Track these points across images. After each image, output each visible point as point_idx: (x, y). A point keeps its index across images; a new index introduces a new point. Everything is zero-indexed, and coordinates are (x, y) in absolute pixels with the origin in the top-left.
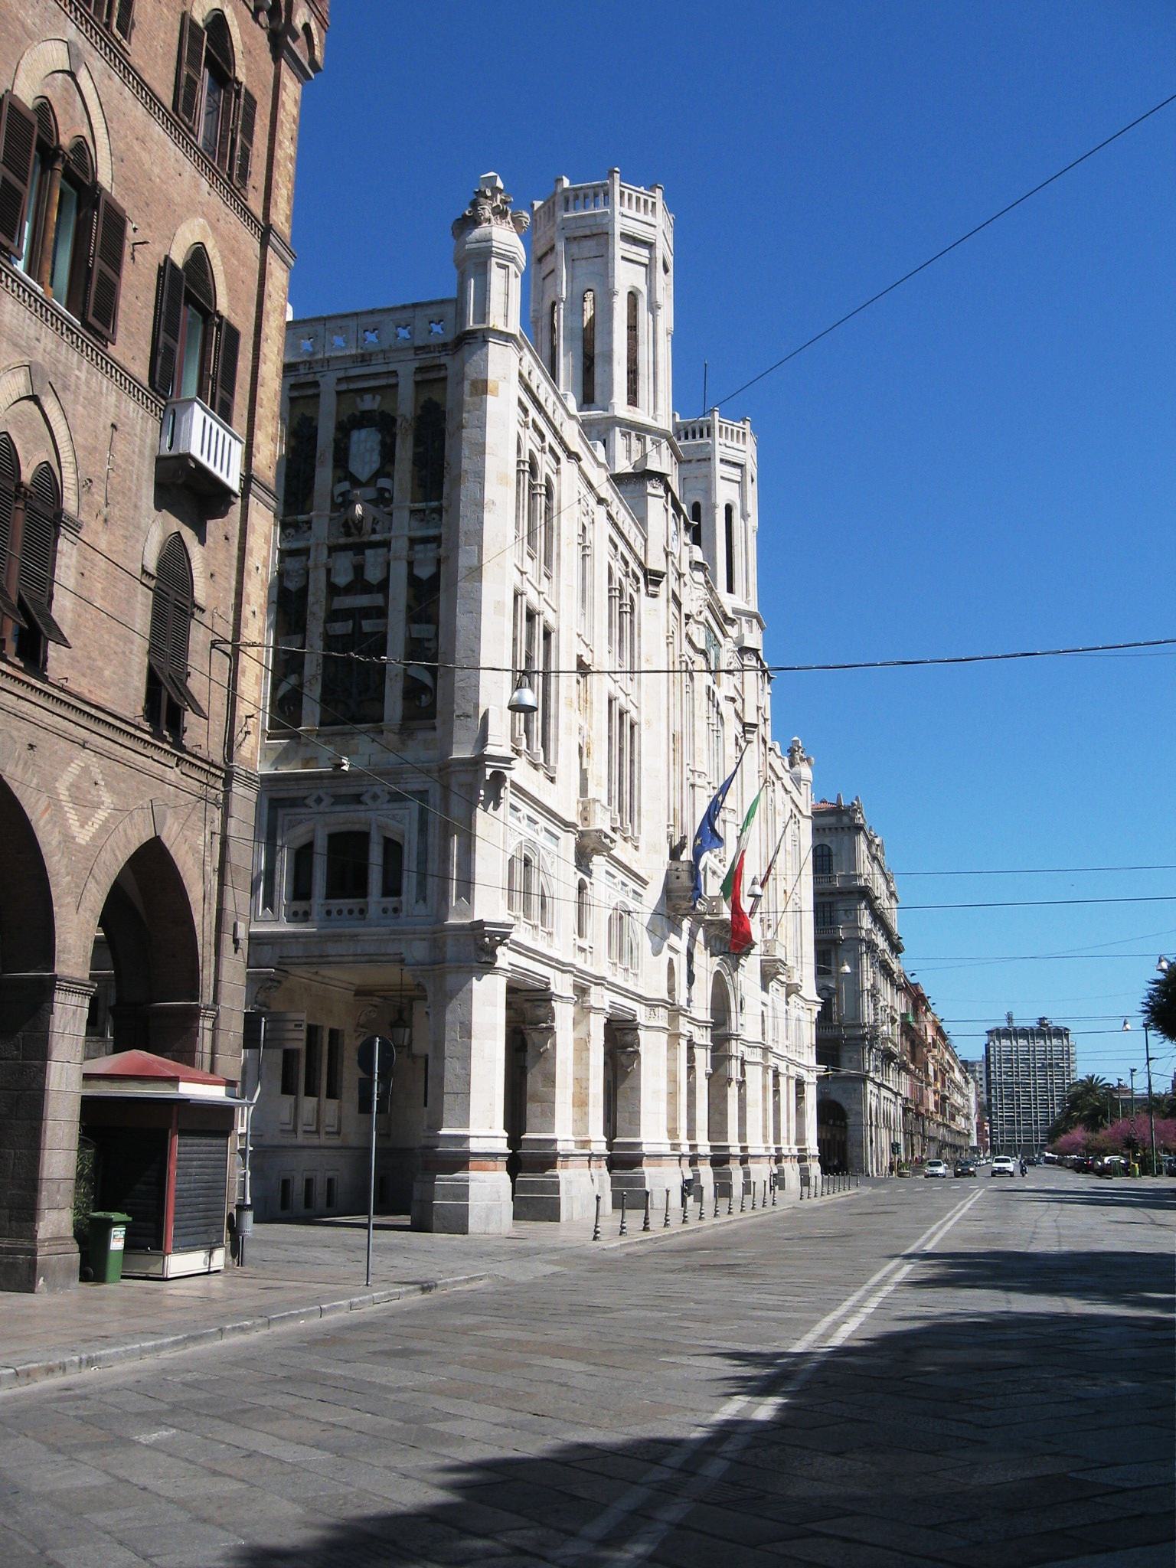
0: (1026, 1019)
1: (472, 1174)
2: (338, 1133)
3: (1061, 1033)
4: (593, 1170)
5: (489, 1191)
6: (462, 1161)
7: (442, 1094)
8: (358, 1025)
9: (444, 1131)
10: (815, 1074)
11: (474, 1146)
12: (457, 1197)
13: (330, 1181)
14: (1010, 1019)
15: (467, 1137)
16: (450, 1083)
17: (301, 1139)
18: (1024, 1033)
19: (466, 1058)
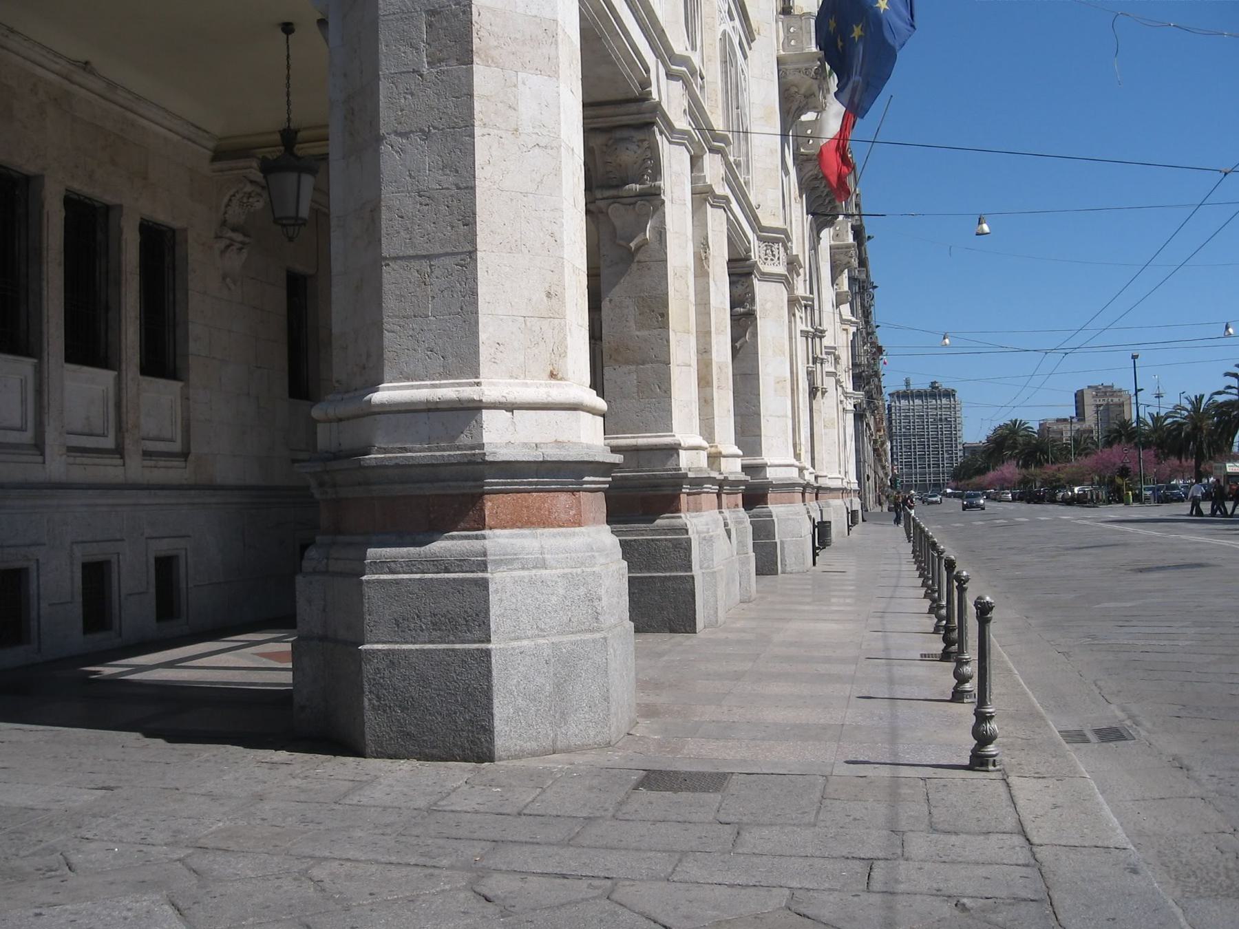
0: (920, 383)
1: (498, 540)
2: (185, 455)
3: (949, 394)
4: (726, 513)
5: (549, 580)
6: (456, 491)
7: (378, 262)
8: (224, 223)
9: (385, 394)
10: (852, 401)
11: (501, 437)
12: (447, 626)
13: (165, 567)
14: (907, 383)
15: (473, 409)
16: (402, 218)
17: (56, 466)
18: (919, 395)
19: (455, 132)
